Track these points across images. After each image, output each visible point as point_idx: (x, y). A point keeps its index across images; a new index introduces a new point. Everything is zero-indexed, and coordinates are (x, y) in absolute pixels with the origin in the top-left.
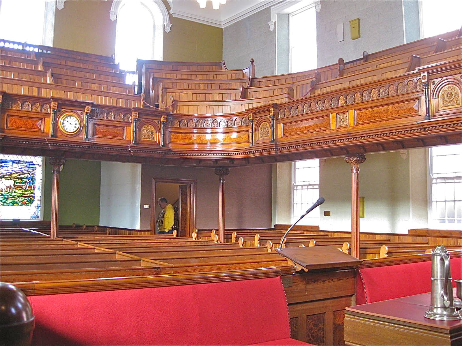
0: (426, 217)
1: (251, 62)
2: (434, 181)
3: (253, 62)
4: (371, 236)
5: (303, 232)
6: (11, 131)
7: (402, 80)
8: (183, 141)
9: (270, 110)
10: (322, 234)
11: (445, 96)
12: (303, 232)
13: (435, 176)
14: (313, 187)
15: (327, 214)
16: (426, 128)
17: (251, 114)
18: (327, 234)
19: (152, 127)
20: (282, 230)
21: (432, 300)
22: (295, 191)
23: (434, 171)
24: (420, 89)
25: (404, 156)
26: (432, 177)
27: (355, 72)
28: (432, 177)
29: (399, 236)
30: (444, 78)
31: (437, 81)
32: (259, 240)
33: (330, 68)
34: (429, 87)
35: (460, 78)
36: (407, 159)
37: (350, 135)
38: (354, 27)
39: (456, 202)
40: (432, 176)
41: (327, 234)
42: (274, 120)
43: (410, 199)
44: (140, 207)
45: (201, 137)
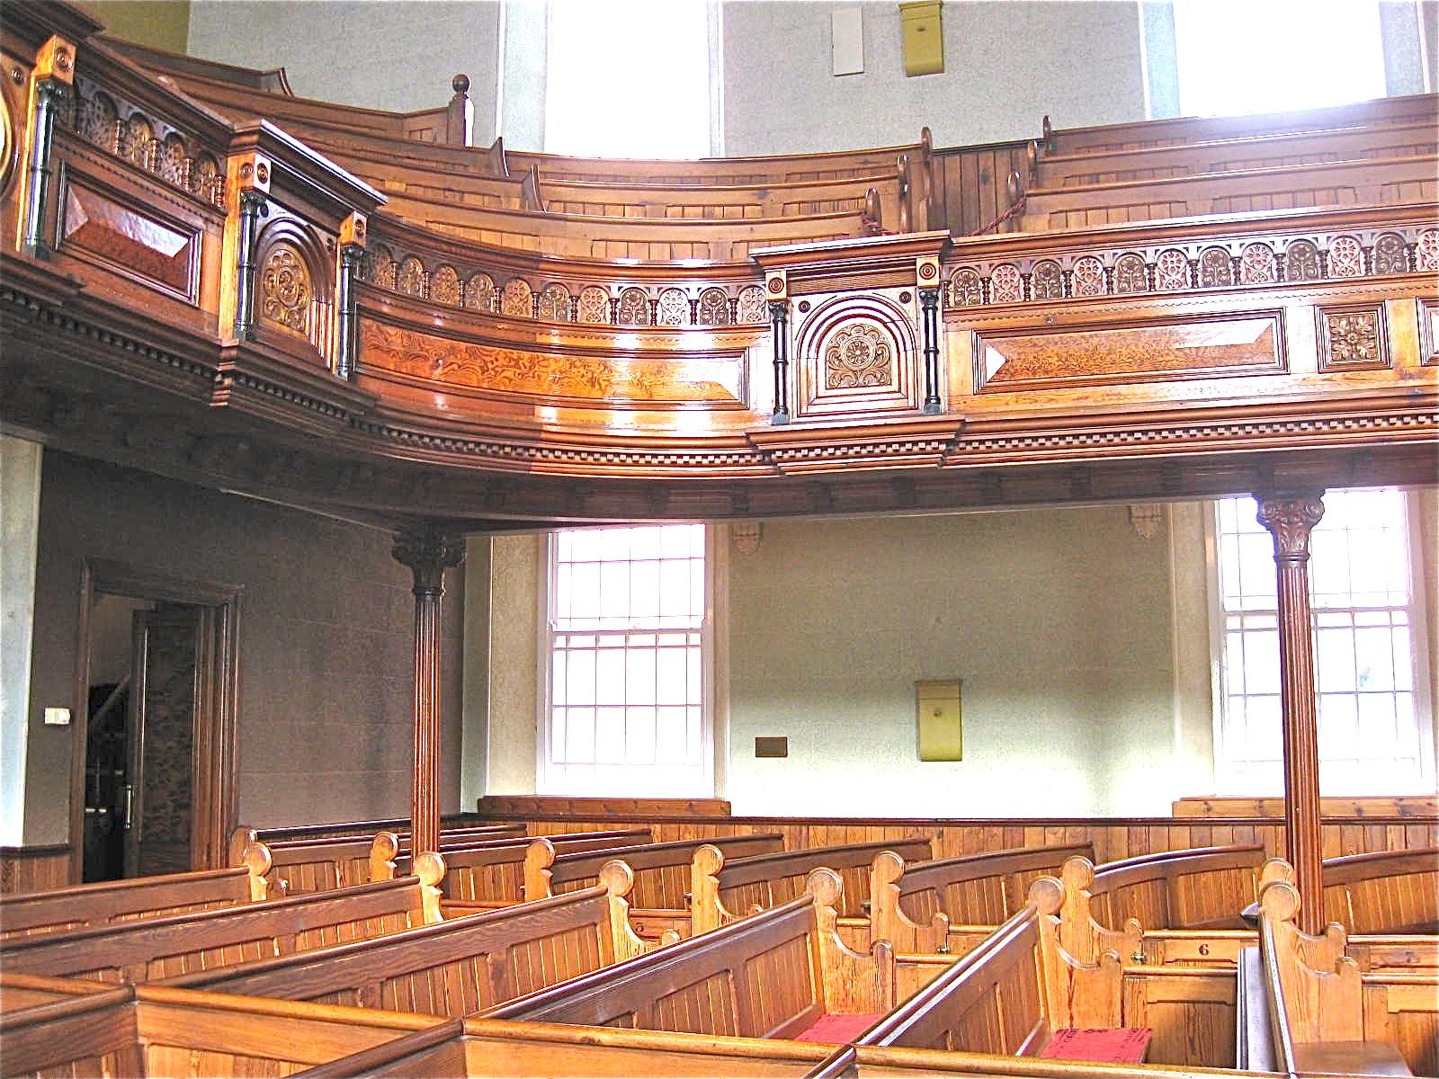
0: (531, 762)
1: (456, 87)
2: (560, 641)
3: (466, 87)
4: (998, 831)
5: (646, 826)
6: (73, 25)
7: (1136, 246)
8: (409, 364)
9: (920, 262)
10: (746, 831)
11: (843, 351)
12: (646, 826)
13: (563, 626)
14: (567, 641)
15: (771, 748)
16: (774, 451)
17: (783, 276)
18: (775, 830)
19: (304, 267)
20: (524, 819)
21: (739, 1053)
22: (559, 657)
23: (563, 610)
24: (1038, 296)
25: (1150, 530)
26: (554, 630)
27: (1102, 177)
28: (554, 630)
29: (1131, 828)
30: (841, 295)
31: (815, 301)
32: (554, 865)
33: (866, 162)
34: (788, 317)
35: (897, 299)
36: (1162, 538)
37: (1417, 401)
38: (922, 30)
39: (600, 709)
40: (554, 626)
41: (775, 830)
42: (935, 309)
43: (1177, 688)
44: (26, 717)
45: (488, 359)
